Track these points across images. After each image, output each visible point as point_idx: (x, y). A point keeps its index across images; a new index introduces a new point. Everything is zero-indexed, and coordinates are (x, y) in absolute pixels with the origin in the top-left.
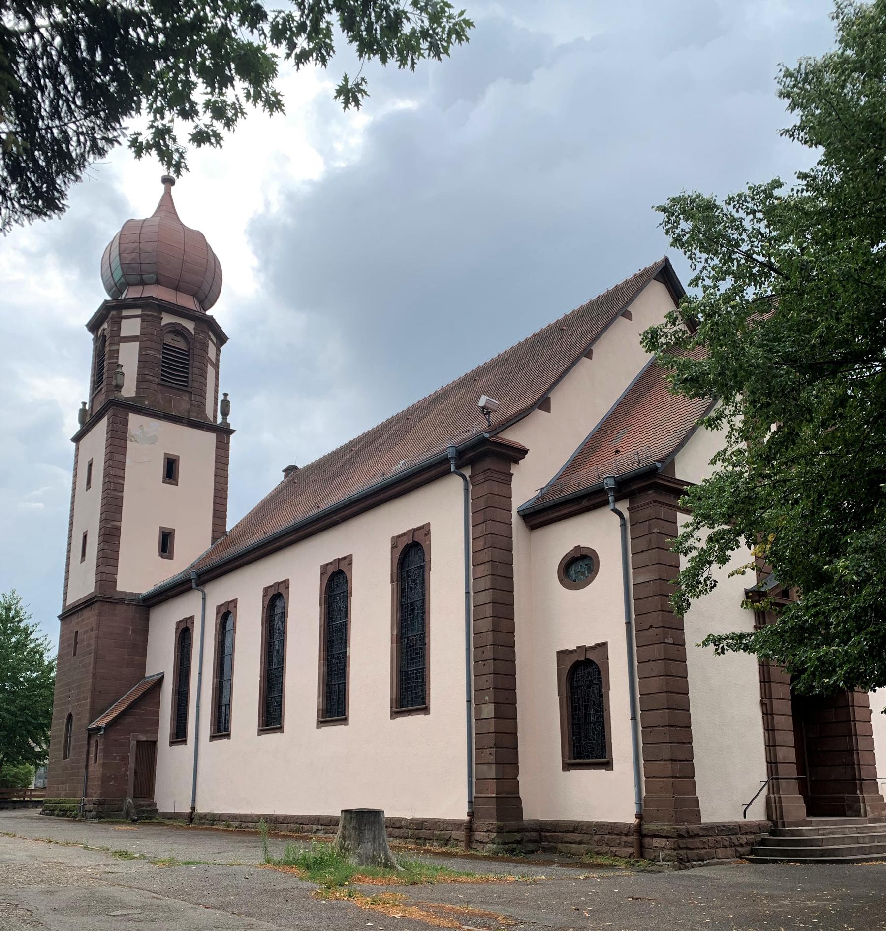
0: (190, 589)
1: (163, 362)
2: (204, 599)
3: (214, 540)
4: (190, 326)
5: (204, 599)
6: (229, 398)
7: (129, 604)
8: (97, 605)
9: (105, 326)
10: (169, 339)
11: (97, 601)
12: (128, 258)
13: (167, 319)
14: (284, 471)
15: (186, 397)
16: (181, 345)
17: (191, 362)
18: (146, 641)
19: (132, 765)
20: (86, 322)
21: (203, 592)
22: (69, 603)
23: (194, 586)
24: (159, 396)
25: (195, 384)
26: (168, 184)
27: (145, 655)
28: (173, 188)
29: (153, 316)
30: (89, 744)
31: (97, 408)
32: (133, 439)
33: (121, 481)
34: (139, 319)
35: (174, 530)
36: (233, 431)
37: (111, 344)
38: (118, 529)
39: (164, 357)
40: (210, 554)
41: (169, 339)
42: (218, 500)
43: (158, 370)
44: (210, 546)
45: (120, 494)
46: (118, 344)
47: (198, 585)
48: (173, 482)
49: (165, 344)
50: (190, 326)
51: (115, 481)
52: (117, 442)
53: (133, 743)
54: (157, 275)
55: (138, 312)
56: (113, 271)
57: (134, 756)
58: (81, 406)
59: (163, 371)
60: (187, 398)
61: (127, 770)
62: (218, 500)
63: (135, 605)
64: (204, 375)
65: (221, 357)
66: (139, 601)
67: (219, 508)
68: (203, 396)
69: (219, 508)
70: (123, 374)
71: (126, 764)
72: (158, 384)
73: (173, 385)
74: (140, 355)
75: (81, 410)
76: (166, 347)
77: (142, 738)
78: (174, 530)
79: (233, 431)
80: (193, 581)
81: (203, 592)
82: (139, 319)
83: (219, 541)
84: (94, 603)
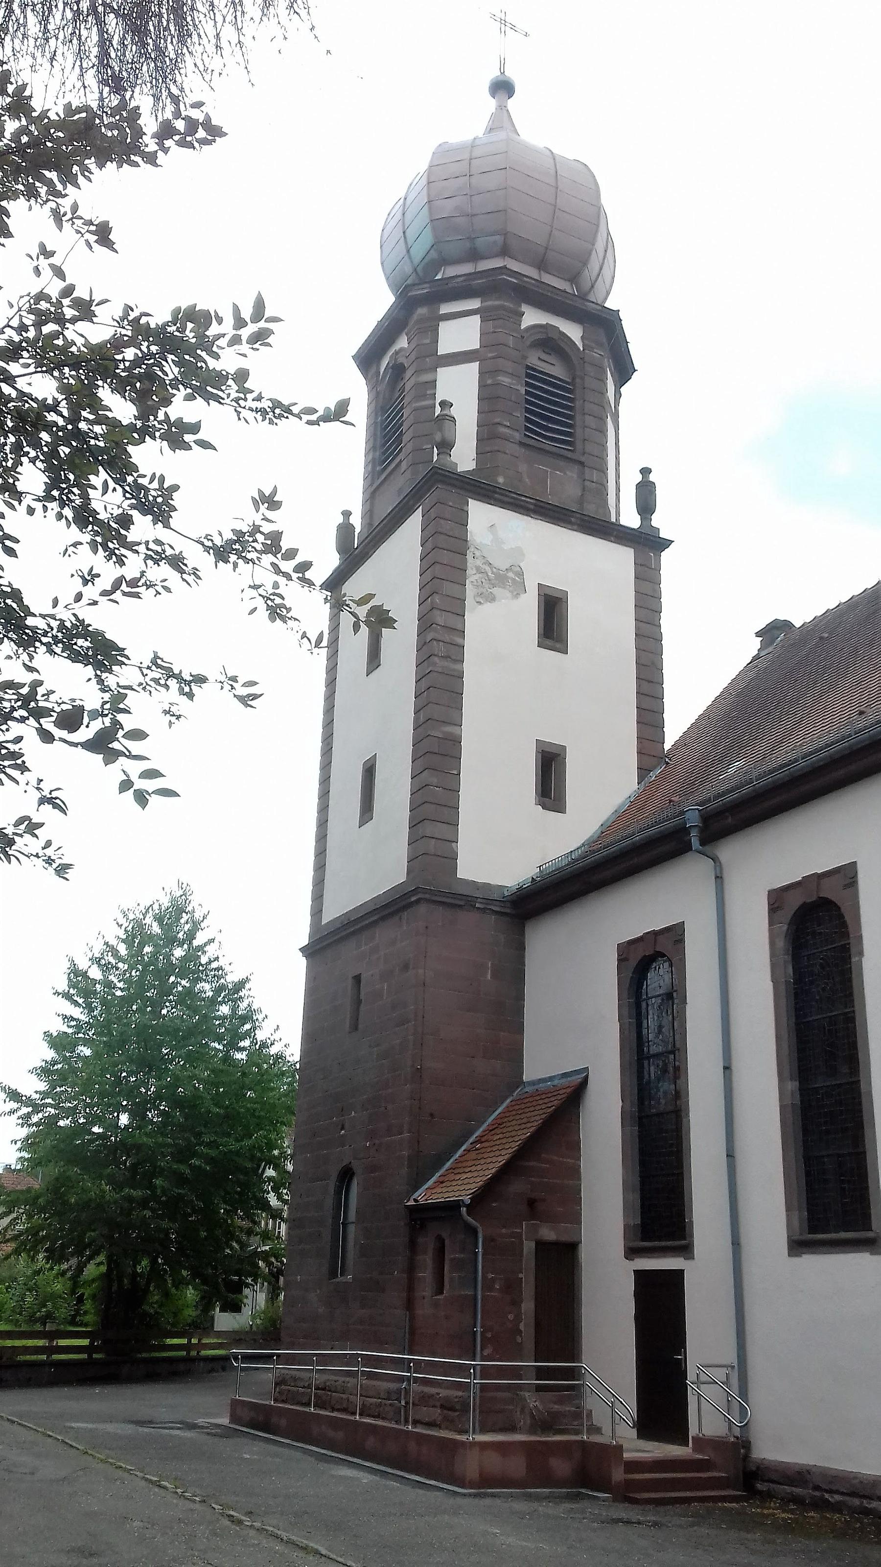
0: (683, 849)
1: (528, 402)
2: (719, 878)
3: (643, 771)
4: (573, 332)
5: (719, 878)
6: (652, 477)
7: (483, 910)
8: (423, 909)
9: (403, 342)
10: (534, 359)
11: (418, 901)
12: (447, 208)
13: (532, 317)
14: (758, 634)
15: (572, 473)
16: (557, 370)
17: (578, 404)
18: (520, 997)
19: (528, 1306)
20: (354, 351)
21: (715, 859)
22: (328, 917)
23: (695, 843)
24: (523, 468)
25: (589, 448)
26: (502, 95)
27: (519, 1029)
28: (511, 103)
29: (502, 307)
30: (413, 1245)
31: (387, 505)
32: (477, 553)
33: (459, 640)
34: (477, 319)
35: (564, 748)
36: (667, 543)
37: (417, 372)
38: (456, 741)
39: (527, 392)
40: (636, 804)
41: (534, 359)
42: (646, 687)
43: (520, 414)
44: (636, 786)
45: (457, 667)
46: (435, 370)
47: (703, 843)
48: (558, 645)
49: (528, 367)
50: (573, 332)
51: (447, 638)
52: (445, 557)
53: (529, 1247)
54: (505, 234)
55: (474, 304)
56: (410, 241)
57: (532, 1279)
58: (340, 519)
59: (527, 420)
60: (575, 476)
61: (518, 1318)
62: (646, 687)
63: (496, 912)
64: (603, 432)
65: (620, 408)
66: (502, 902)
67: (647, 703)
68: (603, 471)
69: (647, 703)
70: (453, 420)
71: (516, 1303)
72: (521, 444)
73: (548, 448)
74: (482, 386)
75: (340, 527)
76: (531, 373)
77: (548, 1234)
78: (564, 748)
79: (667, 543)
80: (694, 833)
81: (715, 859)
82: (477, 319)
83: (653, 775)
84: (410, 905)
